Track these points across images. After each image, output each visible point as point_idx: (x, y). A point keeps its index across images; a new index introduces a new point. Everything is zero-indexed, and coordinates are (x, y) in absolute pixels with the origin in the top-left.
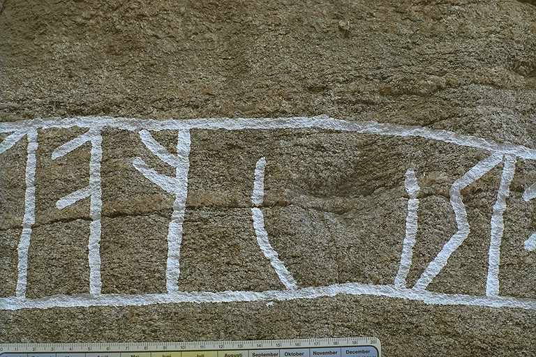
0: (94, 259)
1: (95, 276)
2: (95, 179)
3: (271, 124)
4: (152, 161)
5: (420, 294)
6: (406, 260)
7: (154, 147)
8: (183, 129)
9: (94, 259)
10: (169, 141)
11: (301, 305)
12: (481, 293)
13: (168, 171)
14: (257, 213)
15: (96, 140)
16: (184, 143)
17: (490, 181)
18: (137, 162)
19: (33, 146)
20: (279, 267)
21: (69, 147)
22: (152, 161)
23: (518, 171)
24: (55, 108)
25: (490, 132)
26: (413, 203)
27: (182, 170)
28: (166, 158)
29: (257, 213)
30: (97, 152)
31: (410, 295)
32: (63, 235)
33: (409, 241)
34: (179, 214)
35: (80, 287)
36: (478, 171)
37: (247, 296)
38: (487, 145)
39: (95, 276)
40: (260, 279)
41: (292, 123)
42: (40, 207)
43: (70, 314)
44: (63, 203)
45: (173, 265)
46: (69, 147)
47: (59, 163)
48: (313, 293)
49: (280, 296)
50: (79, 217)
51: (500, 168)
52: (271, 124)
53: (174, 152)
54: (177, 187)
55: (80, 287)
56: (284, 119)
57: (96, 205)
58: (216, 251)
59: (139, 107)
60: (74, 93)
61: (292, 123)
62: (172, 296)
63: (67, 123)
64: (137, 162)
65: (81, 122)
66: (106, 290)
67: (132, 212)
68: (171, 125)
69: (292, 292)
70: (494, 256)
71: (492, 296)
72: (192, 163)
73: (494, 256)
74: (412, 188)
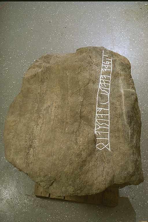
0: (106, 115)
1: (107, 115)
2: (100, 114)
4: (99, 110)
7: (98, 110)
9: (106, 115)
10: (98, 109)
14: (103, 104)
16: (98, 108)
18: (100, 111)
19: (98, 119)
20: (107, 102)
22: (99, 110)
24: (95, 117)
25: (98, 87)
26: (103, 93)
28: (99, 109)
29: (103, 104)
32: (104, 117)
34: (103, 109)
35: (111, 63)
36: (101, 89)
39: (107, 115)
42: (102, 119)
43: (110, 117)
44: (102, 117)
45: (107, 109)
48: (109, 100)
50: (103, 116)
54: (101, 109)
55: (108, 116)
56: (45, 106)
57: (103, 115)
58: (106, 106)
62: (109, 110)
63: (96, 117)
66: (108, 109)
67: (103, 112)
68: (97, 109)
69: (109, 102)
70: (106, 89)
72: (131, 79)
73: (106, 89)
74: (102, 93)
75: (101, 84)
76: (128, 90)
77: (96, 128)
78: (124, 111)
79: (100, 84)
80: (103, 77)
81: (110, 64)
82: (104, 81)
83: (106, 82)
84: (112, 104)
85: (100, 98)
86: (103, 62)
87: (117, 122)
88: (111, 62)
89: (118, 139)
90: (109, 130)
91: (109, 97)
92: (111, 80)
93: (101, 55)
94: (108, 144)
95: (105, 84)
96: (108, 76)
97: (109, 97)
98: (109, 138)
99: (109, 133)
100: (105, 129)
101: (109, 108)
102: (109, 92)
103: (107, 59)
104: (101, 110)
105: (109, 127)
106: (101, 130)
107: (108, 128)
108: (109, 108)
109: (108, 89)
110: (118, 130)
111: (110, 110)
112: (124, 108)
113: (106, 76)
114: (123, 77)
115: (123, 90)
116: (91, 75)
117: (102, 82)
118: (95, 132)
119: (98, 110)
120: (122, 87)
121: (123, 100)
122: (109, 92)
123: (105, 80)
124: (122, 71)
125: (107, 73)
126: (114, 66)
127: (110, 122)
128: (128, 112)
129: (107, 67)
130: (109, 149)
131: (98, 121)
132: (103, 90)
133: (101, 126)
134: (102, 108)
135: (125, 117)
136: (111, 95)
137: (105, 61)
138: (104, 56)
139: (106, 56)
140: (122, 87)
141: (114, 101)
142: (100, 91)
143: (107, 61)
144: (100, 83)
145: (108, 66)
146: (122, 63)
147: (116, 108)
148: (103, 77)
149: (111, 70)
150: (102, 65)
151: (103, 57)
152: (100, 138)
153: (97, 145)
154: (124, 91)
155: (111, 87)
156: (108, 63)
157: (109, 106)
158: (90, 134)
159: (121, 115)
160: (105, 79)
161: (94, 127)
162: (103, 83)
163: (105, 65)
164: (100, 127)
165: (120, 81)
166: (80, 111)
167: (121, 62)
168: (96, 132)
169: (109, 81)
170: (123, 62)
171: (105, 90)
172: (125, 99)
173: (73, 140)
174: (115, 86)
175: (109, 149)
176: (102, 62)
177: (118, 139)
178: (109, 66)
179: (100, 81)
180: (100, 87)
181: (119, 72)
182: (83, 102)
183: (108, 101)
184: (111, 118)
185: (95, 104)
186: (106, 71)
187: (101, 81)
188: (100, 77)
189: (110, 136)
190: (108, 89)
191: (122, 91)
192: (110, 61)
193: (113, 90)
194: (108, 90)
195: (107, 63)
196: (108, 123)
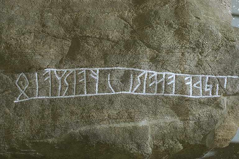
0: (85, 90)
3: (111, 68)
4: (93, 74)
5: (133, 93)
6: (131, 88)
7: (92, 71)
8: (98, 70)
10: (96, 71)
11: (116, 95)
12: (143, 92)
13: (96, 76)
15: (85, 71)
16: (98, 71)
17: (144, 75)
18: (91, 75)
19: (75, 73)
21: (80, 73)
22: (93, 74)
23: (148, 74)
24: (78, 67)
27: (98, 76)
28: (95, 74)
30: (85, 73)
31: (132, 93)
33: (131, 85)
36: (142, 74)
37: (108, 94)
38: (143, 71)
40: (109, 91)
41: (113, 68)
46: (80, 73)
47: (35, 150)
48: (117, 93)
49: (112, 93)
51: (145, 74)
52: (111, 68)
53: (96, 73)
54: (97, 78)
58: (103, 87)
59: (91, 66)
60: (81, 64)
61: (113, 68)
62: (97, 94)
64: (91, 75)
65: (82, 69)
67: (90, 82)
69: (114, 93)
70: (145, 87)
71: (144, 93)
73: (145, 87)
75: (153, 76)
76: (149, 136)
77: (58, 70)
78: (98, 127)
79: (154, 72)
80: (170, 77)
81: (204, 93)
82: (162, 82)
83: (159, 86)
84: (111, 101)
85: (122, 73)
86: (207, 77)
87: (72, 113)
88: (211, 96)
89: (38, 117)
90: (55, 97)
91: (126, 92)
92: (166, 97)
93: (225, 71)
94: (27, 97)
95: (155, 84)
96: (174, 90)
97: (126, 92)
98: (39, 97)
99: (50, 97)
100: (56, 89)
101: (100, 94)
102: (137, 94)
103: (218, 85)
104: (95, 78)
105: (62, 97)
106: (55, 81)
107: (59, 95)
108: (100, 94)
109: (144, 91)
110: (55, 116)
111: (96, 96)
112: (104, 126)
113: (174, 84)
114: (179, 123)
115: (148, 125)
116: (170, 51)
117: (159, 77)
118: (49, 70)
119: (92, 71)
120: (155, 122)
121: (123, 125)
122: (137, 94)
123: (146, 77)
124: (195, 123)
125: (181, 87)
126: (201, 103)
127: (70, 99)
128: (95, 135)
129: (198, 87)
130: (17, 101)
131: (72, 74)
132: (139, 79)
133: (62, 80)
134: (98, 79)
135: (83, 129)
136: (130, 97)
137: (211, 81)
138: (223, 79)
139: (226, 83)
140: (155, 122)
141: (117, 105)
142: (135, 74)
143: (211, 86)
144: (156, 73)
145: (200, 88)
146: (216, 122)
147: (103, 108)
148: (170, 77)
149: (191, 96)
150: (201, 76)
151: (221, 77)
152: (37, 80)
153: (24, 75)
154: (145, 128)
155: (150, 97)
156: (208, 88)
157: (105, 94)
158: (40, 57)
159: (89, 121)
160: (166, 82)
161: (59, 68)
162: (156, 78)
163: (200, 82)
164: (59, 78)
165: (169, 119)
166: (88, 34)
167: (217, 121)
168: (48, 70)
169: (163, 91)
170: (219, 124)
171: (142, 85)
172: (125, 129)
173: (28, 27)
174: (153, 105)
175: (17, 101)
176: (206, 74)
177: (38, 117)
178: (201, 90)
179: (161, 73)
180: (145, 72)
181: (191, 117)
182: (108, 39)
183: (116, 91)
184: (79, 99)
185: (106, 64)
186: (187, 84)
187: (161, 75)
188: (168, 73)
189: (43, 100)
190: (144, 91)
191: (143, 123)
192: (213, 94)
193: (144, 101)
194: (141, 90)
195: (207, 85)
196: (69, 93)
